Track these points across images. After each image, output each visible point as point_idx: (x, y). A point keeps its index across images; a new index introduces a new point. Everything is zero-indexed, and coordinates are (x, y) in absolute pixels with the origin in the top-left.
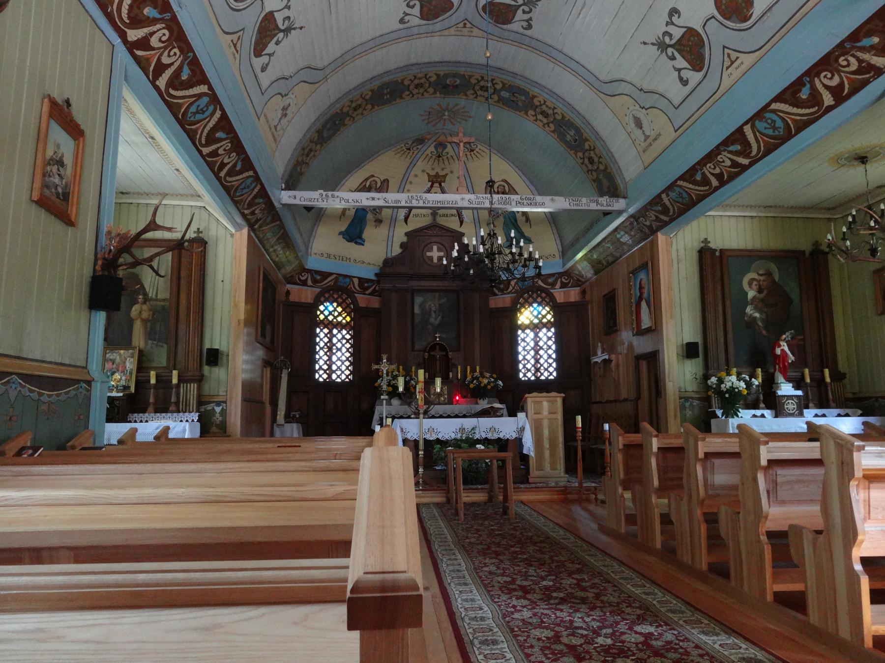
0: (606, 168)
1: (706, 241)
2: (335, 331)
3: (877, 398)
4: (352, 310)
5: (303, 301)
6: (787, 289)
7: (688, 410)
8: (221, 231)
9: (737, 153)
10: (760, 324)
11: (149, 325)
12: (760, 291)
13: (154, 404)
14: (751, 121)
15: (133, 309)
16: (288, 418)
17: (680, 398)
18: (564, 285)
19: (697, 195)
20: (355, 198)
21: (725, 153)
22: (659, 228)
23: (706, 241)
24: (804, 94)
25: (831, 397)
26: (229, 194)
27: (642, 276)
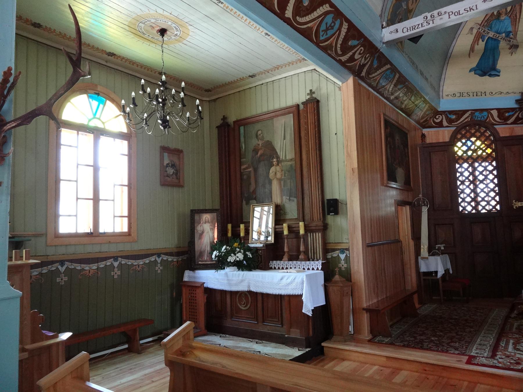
2: (476, 165)
4: (492, 142)
5: (441, 141)
8: (331, 87)
11: (282, 182)
13: (288, 252)
15: (271, 171)
16: (432, 251)
20: (467, 7)
26: (311, 40)
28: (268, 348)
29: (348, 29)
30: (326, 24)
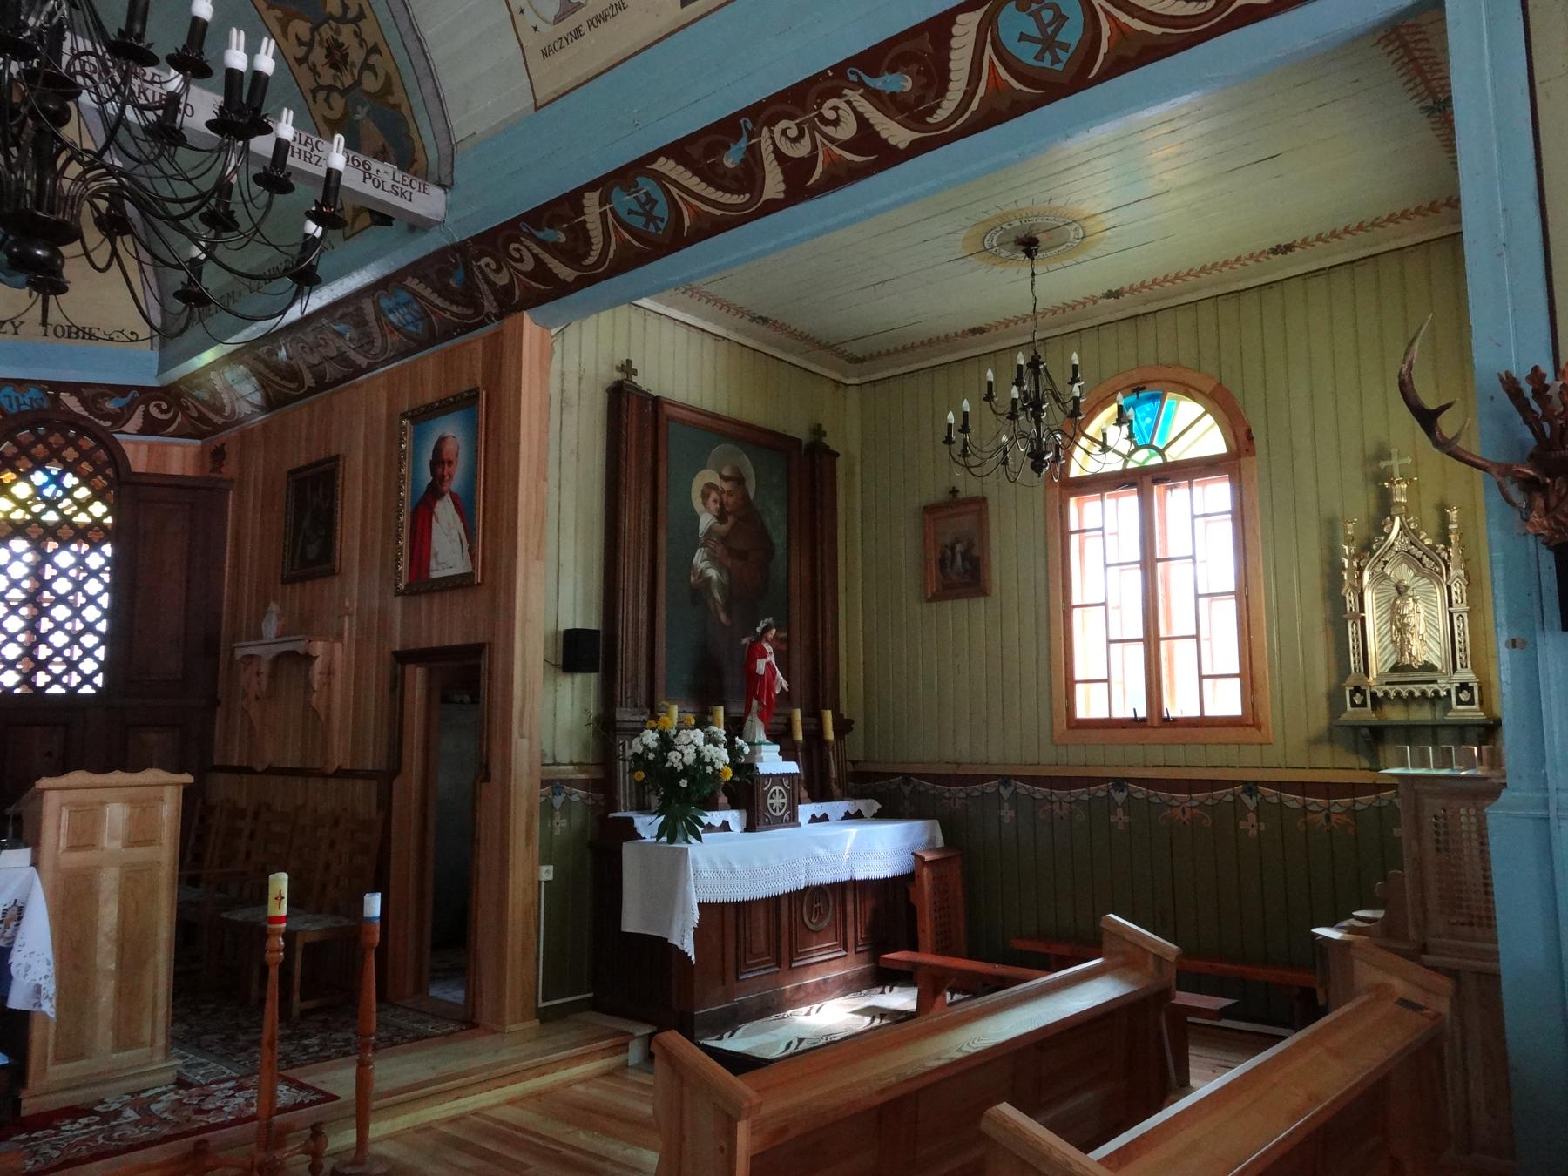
0: (387, 89)
1: (627, 368)
3: (907, 777)
6: (767, 521)
7: (557, 819)
9: (891, 104)
10: (717, 596)
12: (721, 517)
14: (603, 184)
17: (544, 783)
18: (151, 427)
19: (698, 215)
21: (855, 96)
22: (534, 300)
23: (627, 368)
24: (731, 160)
25: (834, 775)
27: (450, 429)
28: (447, 1105)
29: (424, 279)
30: (631, 212)
